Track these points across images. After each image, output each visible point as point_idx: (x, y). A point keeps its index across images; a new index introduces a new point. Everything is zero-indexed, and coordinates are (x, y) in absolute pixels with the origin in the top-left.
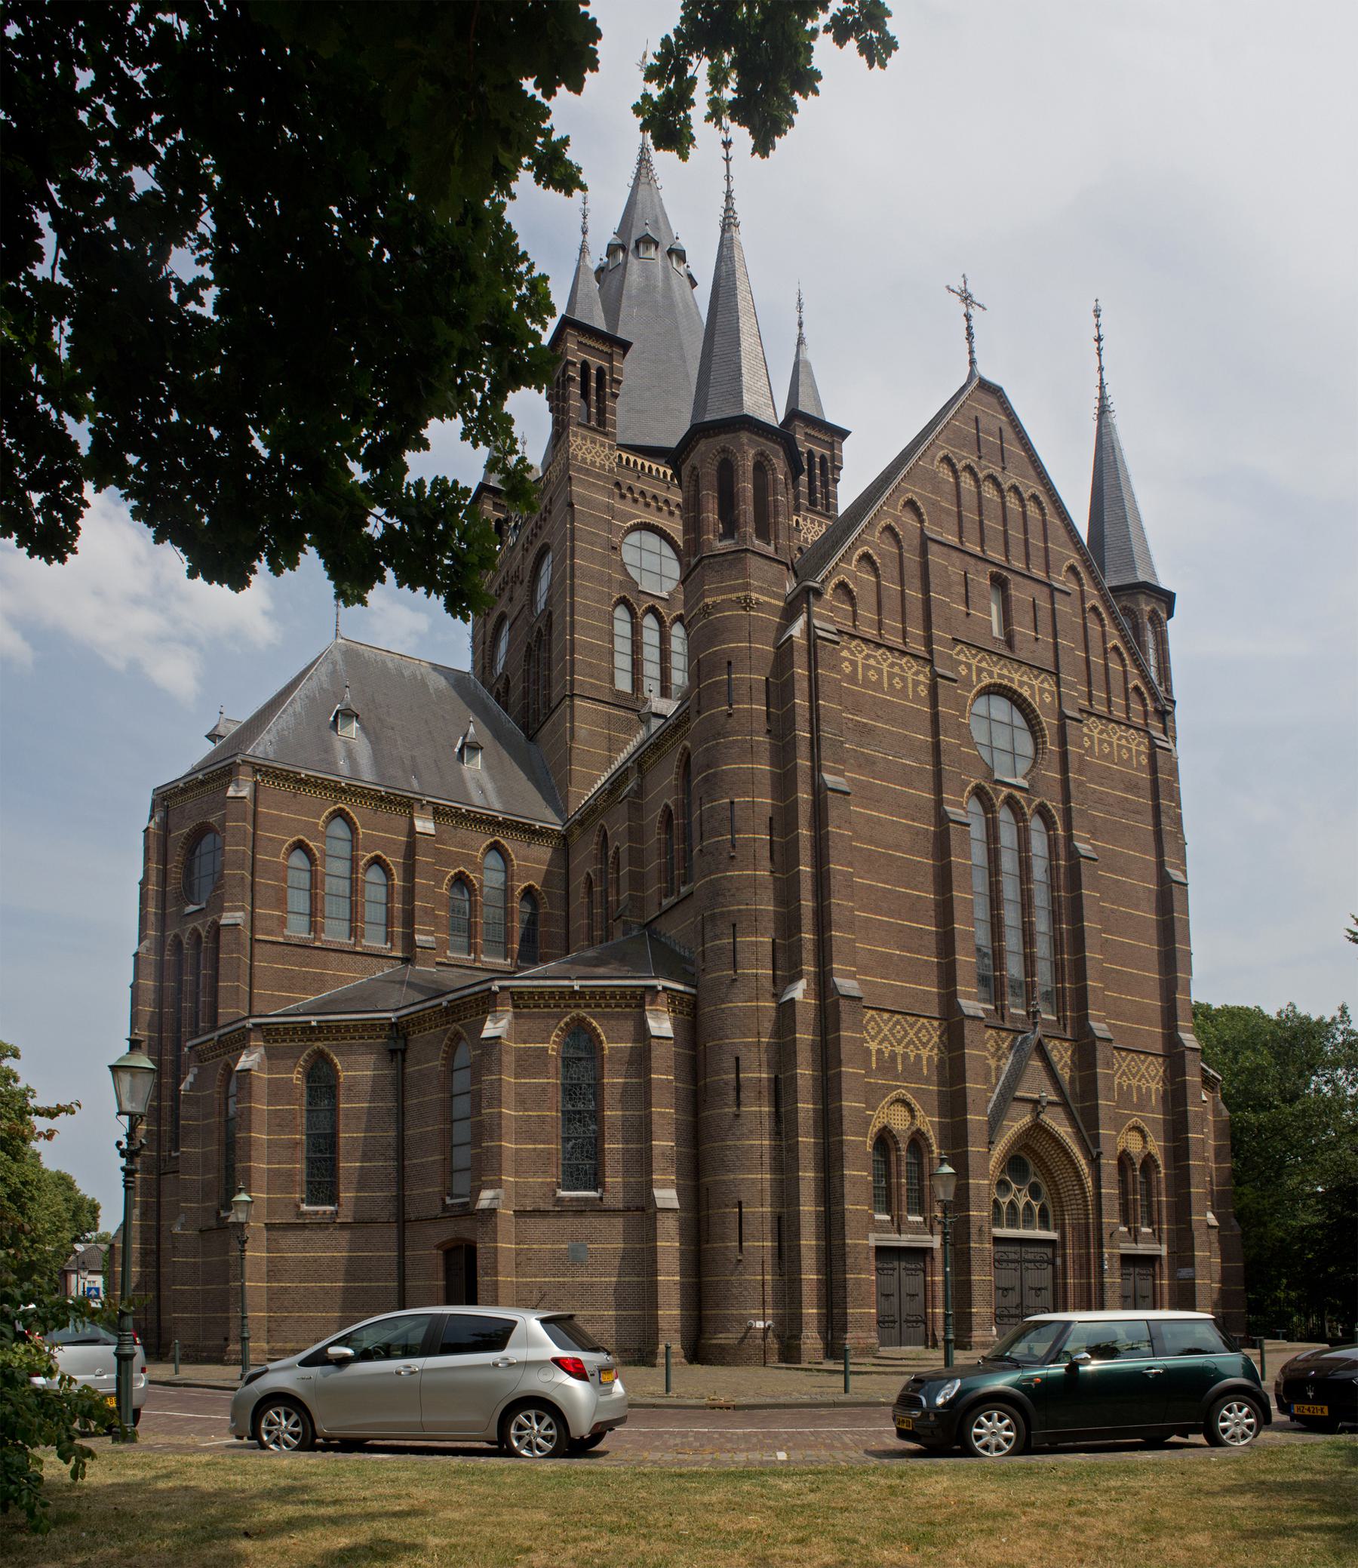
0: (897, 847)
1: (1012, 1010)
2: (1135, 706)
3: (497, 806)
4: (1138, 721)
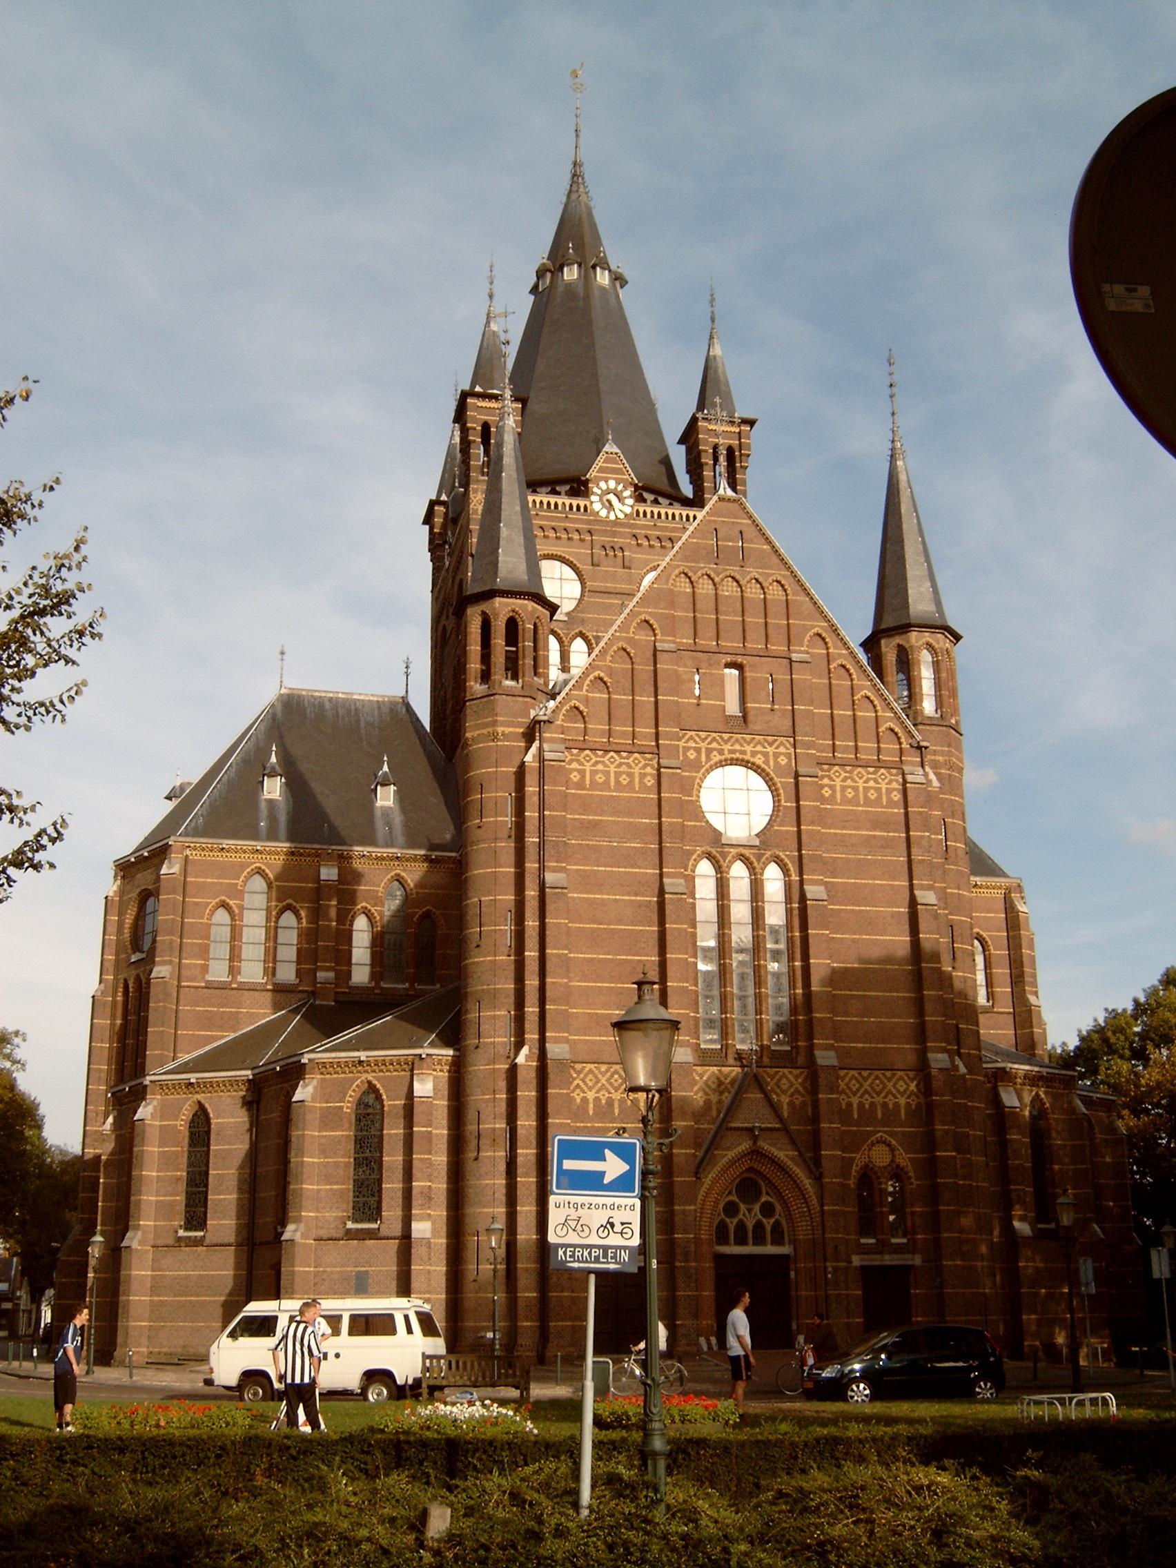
0: (620, 922)
2: (889, 746)
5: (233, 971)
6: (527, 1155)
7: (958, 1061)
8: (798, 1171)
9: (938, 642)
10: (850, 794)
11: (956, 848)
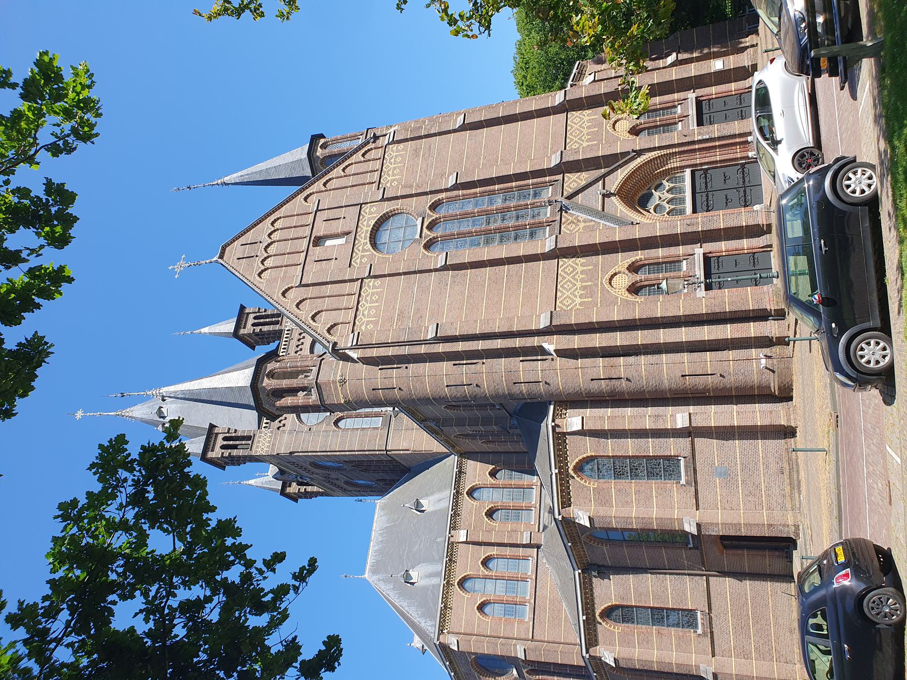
0: (463, 293)
1: (548, 215)
2: (372, 155)
3: (448, 492)
4: (380, 152)
6: (621, 339)
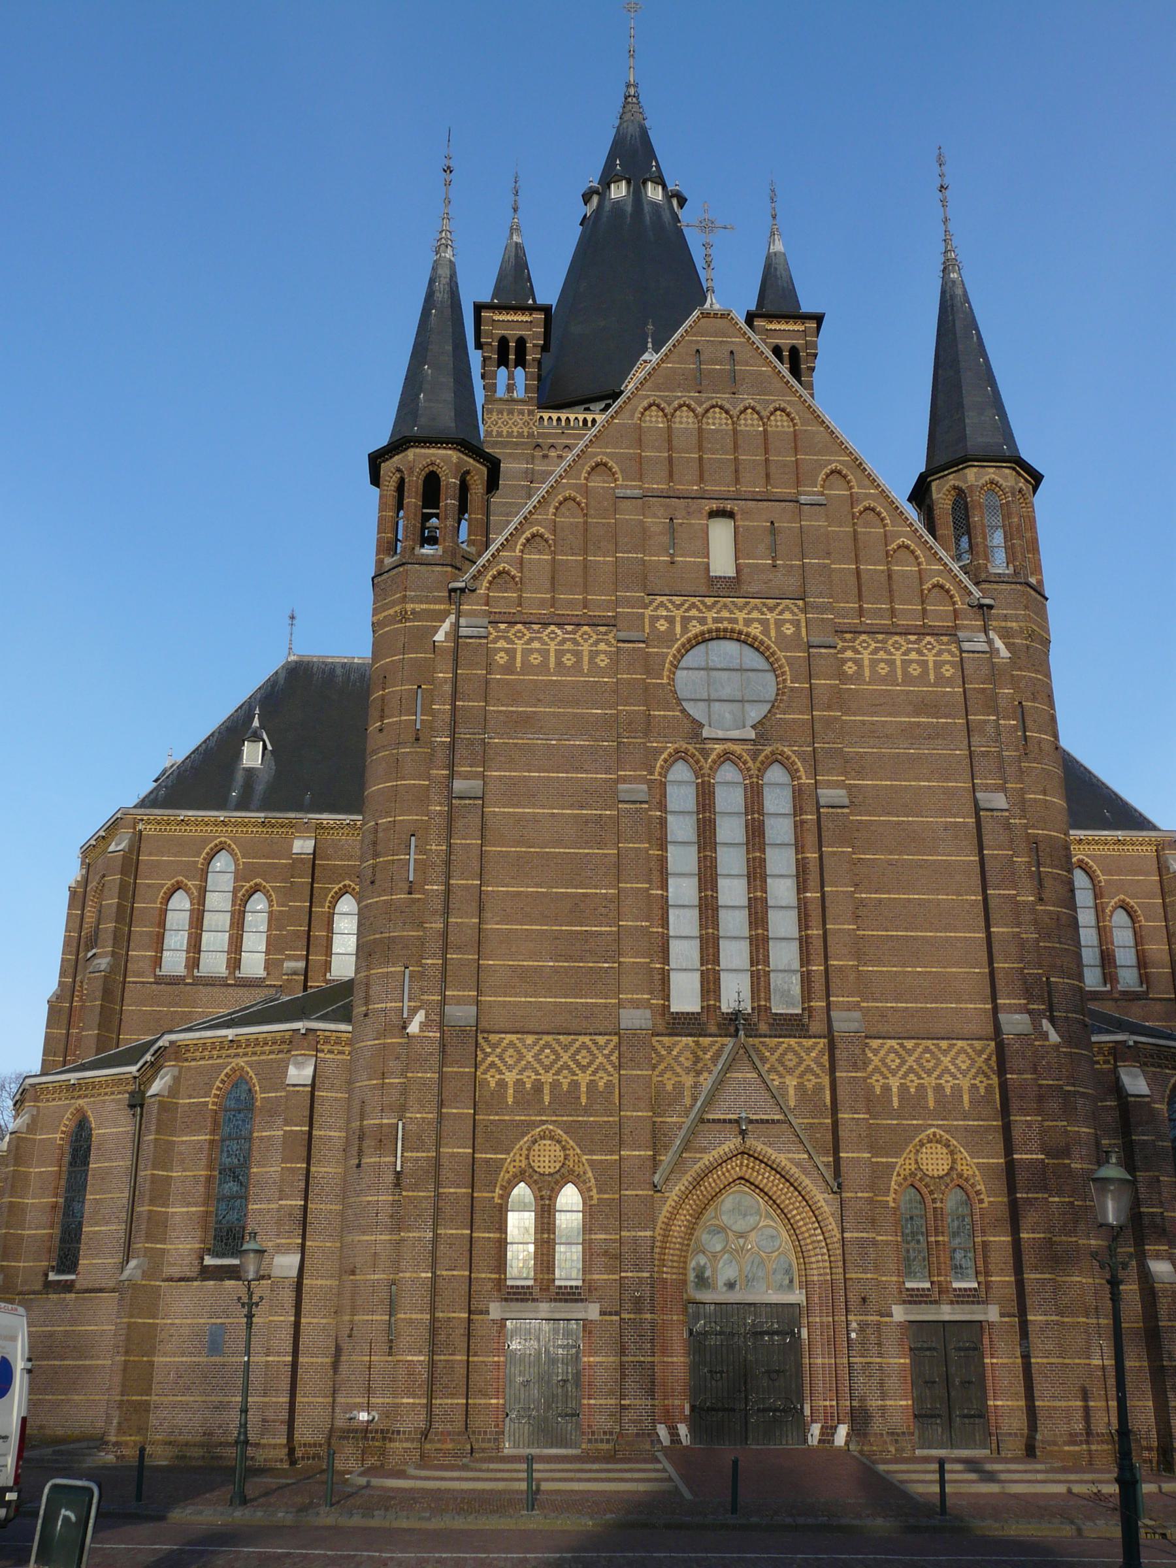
0: (559, 843)
5: (193, 963)
7: (1046, 1025)
8: (807, 1181)
9: (1006, 478)
10: (883, 669)
11: (1040, 741)
